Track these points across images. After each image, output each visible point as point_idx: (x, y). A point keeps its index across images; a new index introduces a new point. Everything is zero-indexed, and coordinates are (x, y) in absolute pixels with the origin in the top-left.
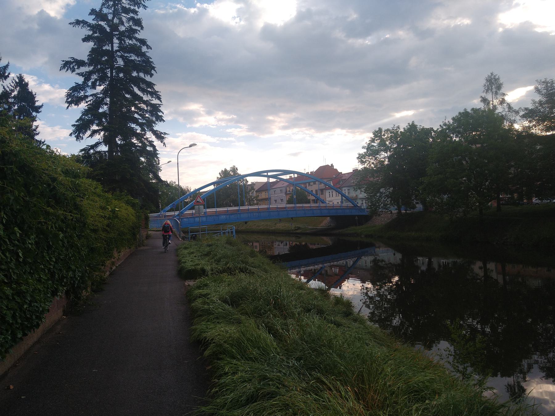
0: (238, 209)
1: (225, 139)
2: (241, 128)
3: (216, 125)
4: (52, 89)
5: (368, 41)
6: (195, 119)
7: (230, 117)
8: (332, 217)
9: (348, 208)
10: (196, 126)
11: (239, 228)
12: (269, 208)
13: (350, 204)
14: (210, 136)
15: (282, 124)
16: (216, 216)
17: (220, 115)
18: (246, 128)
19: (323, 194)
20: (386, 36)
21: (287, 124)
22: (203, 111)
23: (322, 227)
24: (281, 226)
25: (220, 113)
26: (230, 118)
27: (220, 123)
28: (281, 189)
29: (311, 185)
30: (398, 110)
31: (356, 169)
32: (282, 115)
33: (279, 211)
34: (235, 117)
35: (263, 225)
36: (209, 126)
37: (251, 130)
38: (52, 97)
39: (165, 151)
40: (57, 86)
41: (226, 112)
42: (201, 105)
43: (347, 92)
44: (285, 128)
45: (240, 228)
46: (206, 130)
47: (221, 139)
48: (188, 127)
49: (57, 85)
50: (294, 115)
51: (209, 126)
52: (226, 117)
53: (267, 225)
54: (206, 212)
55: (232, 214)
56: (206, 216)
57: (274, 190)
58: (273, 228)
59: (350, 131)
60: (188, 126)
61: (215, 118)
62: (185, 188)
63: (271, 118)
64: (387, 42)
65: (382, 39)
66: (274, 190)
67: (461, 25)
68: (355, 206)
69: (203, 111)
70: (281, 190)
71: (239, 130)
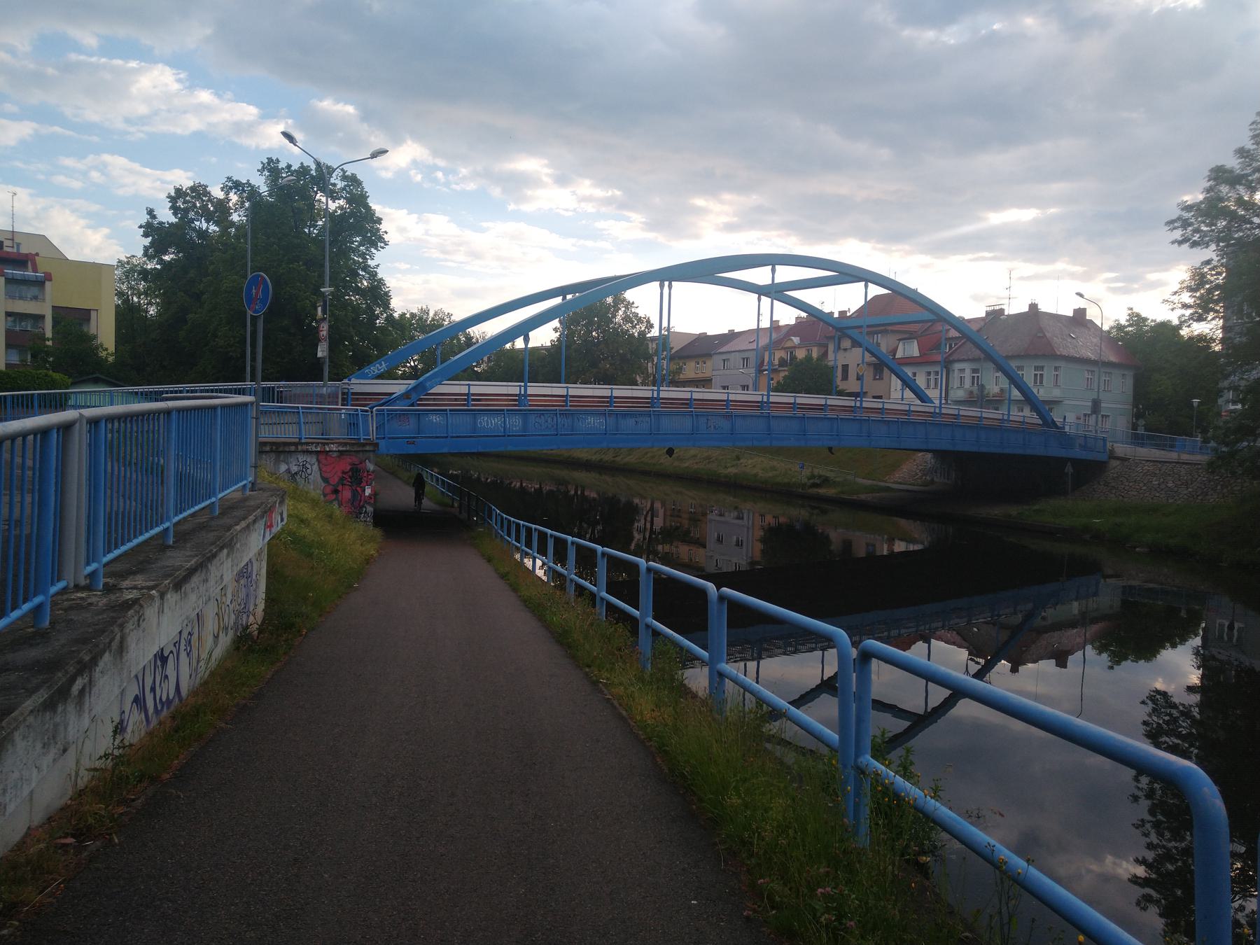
0: (652, 398)
1: (590, 243)
2: (631, 222)
3: (575, 210)
4: (216, 101)
5: (952, 36)
6: (529, 193)
7: (608, 192)
8: (941, 455)
9: (1023, 429)
10: (527, 208)
11: (618, 459)
12: (768, 402)
13: (1033, 418)
14: (557, 234)
15: (724, 219)
16: (565, 414)
17: (586, 187)
18: (641, 223)
19: (881, 378)
20: (995, 27)
21: (735, 219)
22: (547, 175)
23: (900, 483)
24: (756, 466)
25: (587, 182)
26: (607, 195)
27: (583, 205)
28: (746, 355)
29: (845, 350)
30: (997, 205)
31: (997, 308)
32: (727, 197)
33: (841, 419)
34: (618, 193)
35: (695, 456)
36: (558, 210)
37: (651, 226)
38: (214, 119)
39: (452, 261)
40: (229, 95)
41: (602, 182)
42: (546, 161)
43: (885, 153)
44: (730, 228)
45: (622, 459)
46: (548, 220)
47: (582, 242)
48: (510, 210)
49: (229, 93)
50: (754, 199)
51: (558, 210)
52: (599, 193)
53: (708, 458)
54: (526, 395)
55: (625, 415)
56: (525, 414)
57: (724, 357)
58: (732, 470)
59: (881, 246)
60: (512, 207)
61: (574, 193)
62: (478, 337)
63: (700, 202)
64: (993, 40)
65: (983, 32)
66: (724, 357)
67: (1179, 10)
68: (1049, 423)
69: (547, 175)
70: (744, 359)
71: (624, 224)
